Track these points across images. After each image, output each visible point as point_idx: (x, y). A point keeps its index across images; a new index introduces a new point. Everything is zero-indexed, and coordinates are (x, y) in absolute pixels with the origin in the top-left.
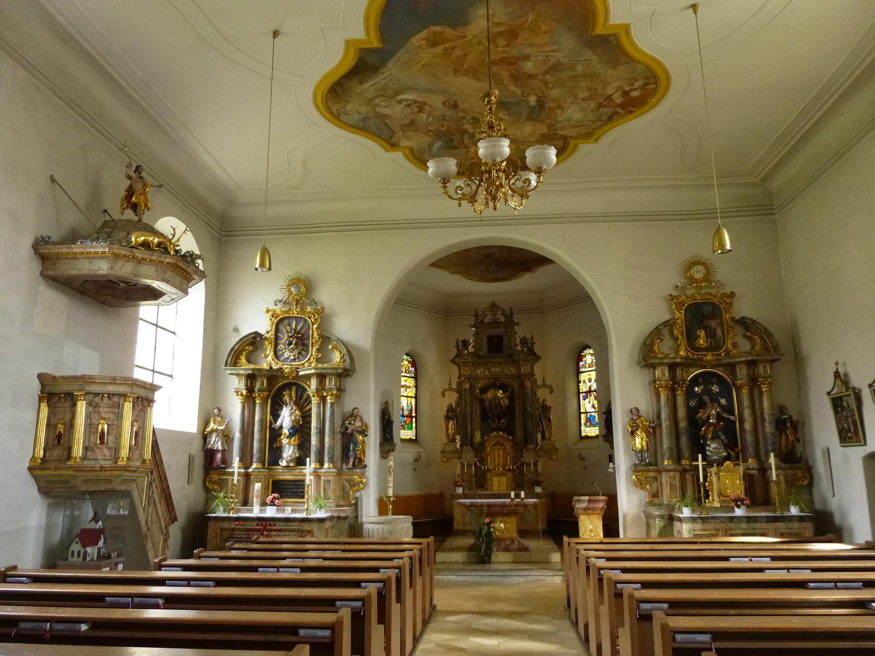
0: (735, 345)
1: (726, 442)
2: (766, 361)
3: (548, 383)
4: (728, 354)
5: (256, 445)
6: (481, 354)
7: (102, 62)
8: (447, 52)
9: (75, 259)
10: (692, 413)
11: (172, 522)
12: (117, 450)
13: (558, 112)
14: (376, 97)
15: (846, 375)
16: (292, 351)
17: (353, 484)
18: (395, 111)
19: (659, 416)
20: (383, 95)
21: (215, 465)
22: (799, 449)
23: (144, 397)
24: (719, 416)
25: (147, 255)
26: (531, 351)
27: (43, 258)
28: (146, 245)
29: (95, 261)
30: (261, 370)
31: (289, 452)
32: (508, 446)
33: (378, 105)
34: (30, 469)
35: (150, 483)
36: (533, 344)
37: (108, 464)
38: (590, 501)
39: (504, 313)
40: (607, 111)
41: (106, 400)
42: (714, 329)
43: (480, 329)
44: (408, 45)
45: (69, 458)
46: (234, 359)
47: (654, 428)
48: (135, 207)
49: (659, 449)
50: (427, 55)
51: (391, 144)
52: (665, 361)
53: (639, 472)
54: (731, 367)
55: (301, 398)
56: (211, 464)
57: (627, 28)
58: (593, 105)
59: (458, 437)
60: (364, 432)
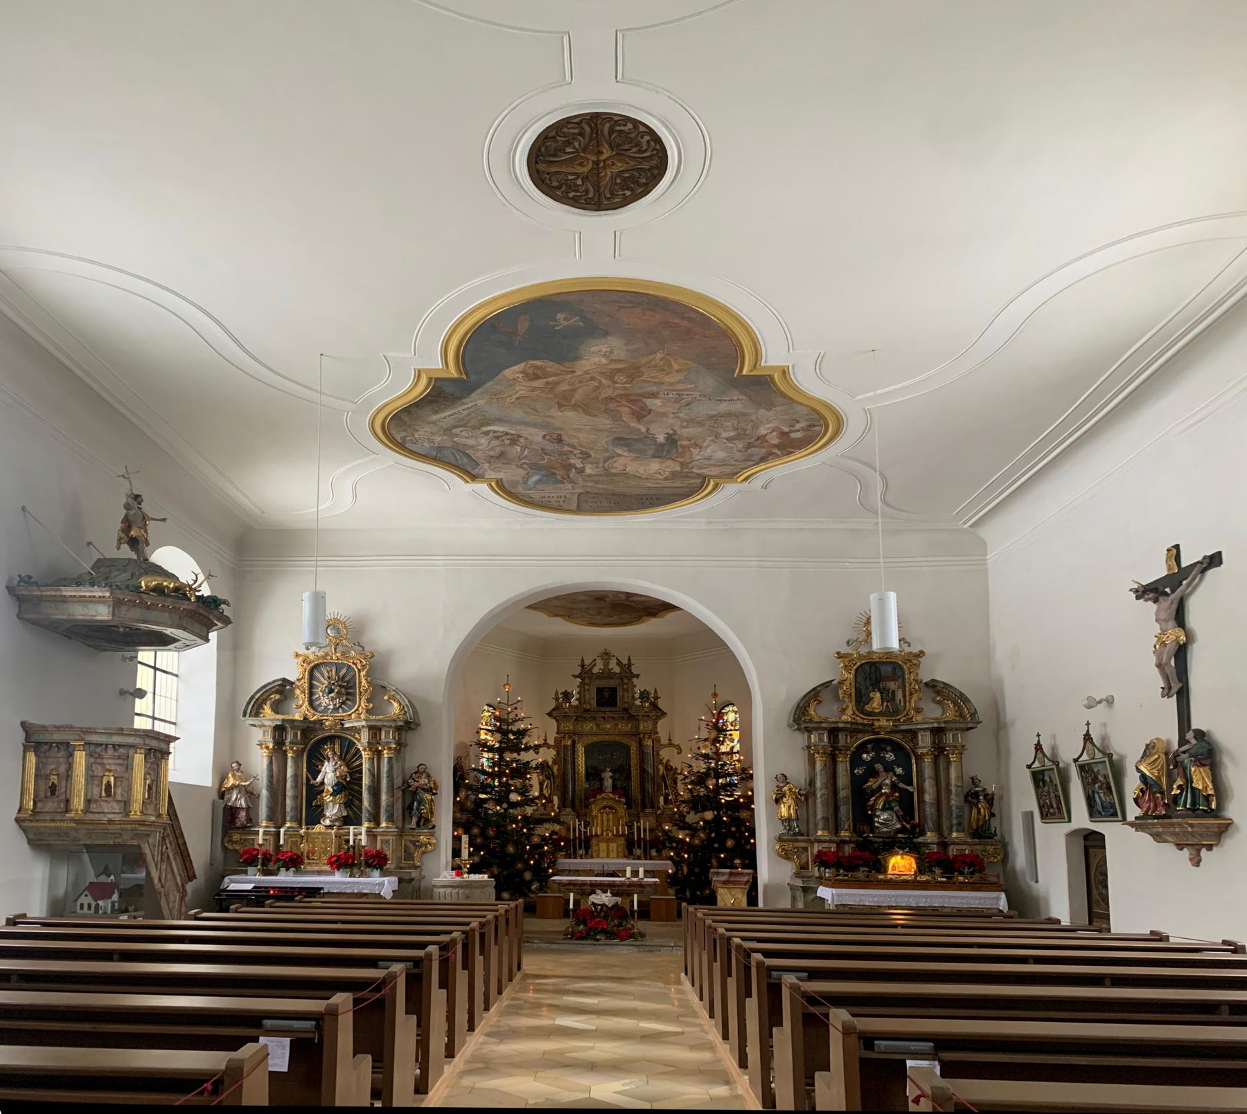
0: (918, 710)
1: (901, 813)
2: (957, 729)
3: (676, 742)
4: (910, 720)
5: (289, 802)
6: (588, 707)
7: (123, 411)
8: (551, 387)
9: (64, 602)
10: (857, 785)
11: (190, 880)
12: (126, 804)
13: (695, 451)
14: (455, 427)
15: (1104, 738)
16: (333, 699)
17: (417, 845)
18: (482, 444)
19: (812, 782)
20: (464, 426)
21: (238, 824)
22: (994, 823)
23: (157, 748)
24: (894, 786)
25: (160, 602)
26: (655, 706)
27: (20, 600)
28: (159, 590)
29: (90, 606)
30: (293, 721)
31: (333, 810)
32: (622, 810)
33: (457, 435)
34: (17, 820)
35: (164, 839)
36: (657, 698)
37: (117, 818)
38: (731, 874)
39: (619, 663)
40: (759, 452)
41: (110, 752)
42: (893, 692)
43: (587, 681)
44: (500, 377)
45: (67, 810)
46: (255, 708)
47: (807, 797)
48: (134, 543)
49: (811, 819)
50: (522, 389)
51: (470, 474)
52: (823, 725)
53: (785, 841)
54: (914, 733)
55: (347, 752)
56: (230, 820)
57: (784, 372)
58: (740, 445)
59: (555, 799)
60: (432, 790)
